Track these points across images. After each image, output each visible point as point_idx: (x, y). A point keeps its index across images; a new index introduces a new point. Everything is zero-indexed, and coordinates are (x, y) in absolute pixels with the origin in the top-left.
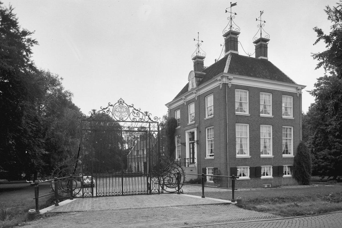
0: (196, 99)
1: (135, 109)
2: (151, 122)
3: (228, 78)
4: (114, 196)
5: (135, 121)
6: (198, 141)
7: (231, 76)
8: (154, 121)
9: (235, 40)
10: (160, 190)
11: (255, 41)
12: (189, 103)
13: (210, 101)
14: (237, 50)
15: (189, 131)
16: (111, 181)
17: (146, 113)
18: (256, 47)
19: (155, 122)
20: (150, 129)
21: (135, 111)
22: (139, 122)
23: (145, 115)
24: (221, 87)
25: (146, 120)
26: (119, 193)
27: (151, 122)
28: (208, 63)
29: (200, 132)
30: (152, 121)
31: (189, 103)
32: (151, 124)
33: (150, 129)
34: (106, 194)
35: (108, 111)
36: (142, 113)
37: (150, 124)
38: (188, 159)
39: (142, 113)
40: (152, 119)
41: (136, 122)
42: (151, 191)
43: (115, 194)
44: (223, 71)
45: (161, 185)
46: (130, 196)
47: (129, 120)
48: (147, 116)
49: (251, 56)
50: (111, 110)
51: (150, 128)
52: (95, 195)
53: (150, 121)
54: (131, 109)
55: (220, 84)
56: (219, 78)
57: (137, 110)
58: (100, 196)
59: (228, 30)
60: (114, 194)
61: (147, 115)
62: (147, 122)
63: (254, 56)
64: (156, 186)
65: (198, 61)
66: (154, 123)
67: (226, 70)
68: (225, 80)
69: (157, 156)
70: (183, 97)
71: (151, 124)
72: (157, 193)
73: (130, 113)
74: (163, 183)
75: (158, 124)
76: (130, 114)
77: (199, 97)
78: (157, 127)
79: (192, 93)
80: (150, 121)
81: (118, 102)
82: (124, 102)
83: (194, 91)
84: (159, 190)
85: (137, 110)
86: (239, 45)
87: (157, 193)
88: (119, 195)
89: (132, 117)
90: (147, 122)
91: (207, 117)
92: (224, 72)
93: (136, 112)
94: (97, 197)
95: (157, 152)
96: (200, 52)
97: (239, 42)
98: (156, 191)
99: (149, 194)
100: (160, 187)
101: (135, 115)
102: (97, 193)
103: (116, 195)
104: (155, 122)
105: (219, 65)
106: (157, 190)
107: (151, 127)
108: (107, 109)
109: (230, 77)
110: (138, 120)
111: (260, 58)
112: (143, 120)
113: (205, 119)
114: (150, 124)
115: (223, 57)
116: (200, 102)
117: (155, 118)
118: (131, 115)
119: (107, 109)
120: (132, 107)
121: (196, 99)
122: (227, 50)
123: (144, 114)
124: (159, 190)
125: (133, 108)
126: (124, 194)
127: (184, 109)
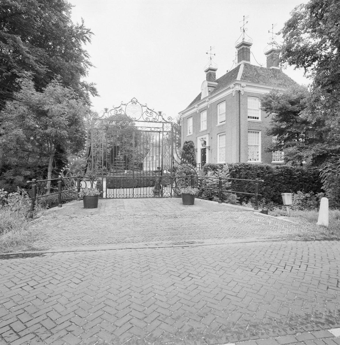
0: (209, 107)
1: (148, 109)
2: (165, 123)
3: (240, 86)
4: (124, 198)
5: (148, 121)
6: (210, 147)
7: (243, 84)
8: (168, 121)
9: (247, 51)
10: (172, 194)
11: (265, 52)
12: (201, 111)
13: (222, 107)
14: (249, 60)
15: (201, 137)
16: (133, 190)
17: (160, 112)
18: (267, 58)
19: (169, 123)
20: (163, 130)
21: (148, 110)
22: (152, 122)
23: (159, 115)
24: (234, 94)
25: (159, 120)
26: (137, 195)
27: (165, 123)
28: (219, 75)
29: (212, 138)
30: (166, 121)
31: (201, 111)
32: (164, 124)
33: (163, 130)
34: (140, 196)
35: (121, 110)
36: (155, 112)
37: (163, 124)
38: (199, 164)
39: (155, 112)
40: (166, 119)
41: (150, 122)
42: (163, 194)
43: (136, 196)
44: (236, 78)
45: (174, 188)
46: (128, 329)
47: (141, 119)
48: (107, 112)
49: (262, 66)
50: (124, 109)
51: (163, 128)
52: (104, 196)
53: (163, 121)
54: (145, 109)
55: (233, 91)
56: (232, 85)
57: (151, 110)
58: (110, 198)
59: (240, 41)
60: (124, 196)
61: (160, 115)
62: (160, 122)
63: (265, 66)
64: (168, 189)
65: (210, 73)
66: (168, 124)
67: (239, 78)
68: (238, 88)
69: (170, 158)
70: (196, 106)
71: (164, 124)
72: (170, 197)
73: (143, 112)
74: (176, 186)
75: (172, 124)
76: (143, 112)
77: (211, 105)
78: (171, 127)
79: (205, 102)
80: (163, 121)
81: (132, 101)
82: (137, 102)
83: (207, 100)
84: (171, 194)
85: (151, 110)
86: (251, 55)
87: (170, 197)
88: (129, 198)
89: (145, 116)
90: (160, 122)
91: (219, 124)
92: (237, 79)
93: (149, 111)
94: (106, 198)
95: (170, 153)
96: (212, 64)
97: (251, 53)
98: (168, 194)
99: (161, 198)
100: (173, 191)
101: (149, 115)
102: (106, 195)
103: (126, 198)
104: (169, 123)
105: (231, 76)
106: (169, 194)
107: (164, 127)
108: (120, 108)
109: (242, 85)
110: (151, 120)
111: (271, 68)
112: (156, 120)
113: (217, 126)
114: (163, 124)
115: (235, 67)
116: (212, 111)
117: (169, 119)
118: (144, 114)
119: (120, 108)
120: (145, 106)
121: (209, 107)
122: (239, 61)
123: (158, 114)
124: (171, 194)
125: (146, 108)
126: (135, 196)
127: (196, 117)
